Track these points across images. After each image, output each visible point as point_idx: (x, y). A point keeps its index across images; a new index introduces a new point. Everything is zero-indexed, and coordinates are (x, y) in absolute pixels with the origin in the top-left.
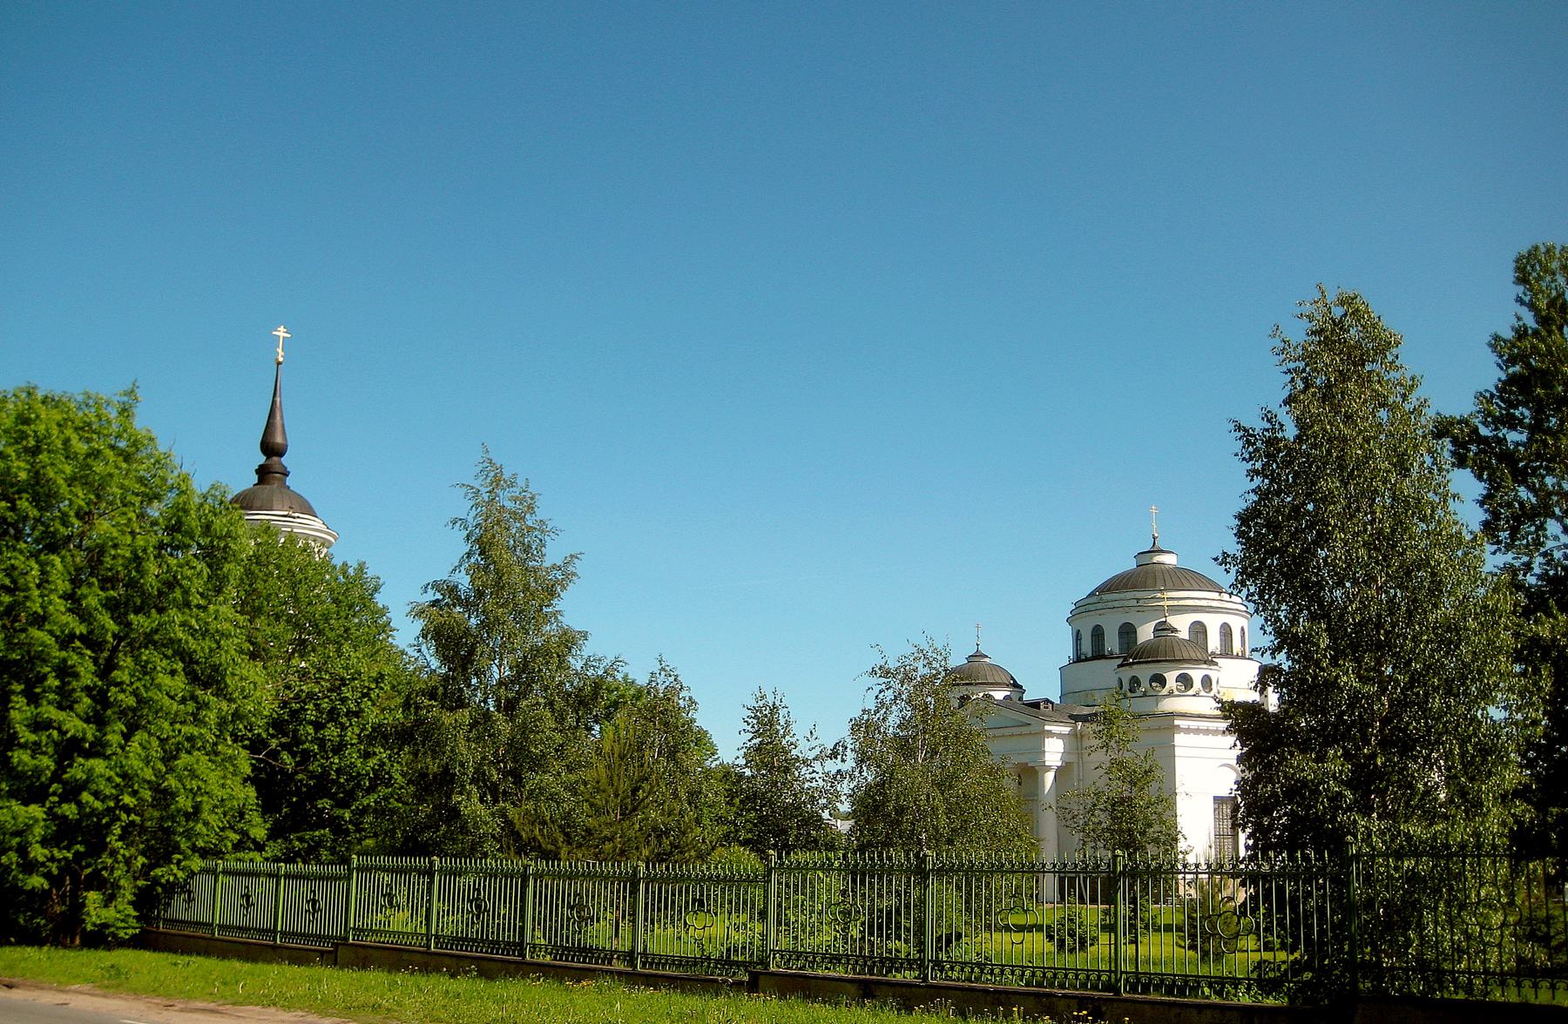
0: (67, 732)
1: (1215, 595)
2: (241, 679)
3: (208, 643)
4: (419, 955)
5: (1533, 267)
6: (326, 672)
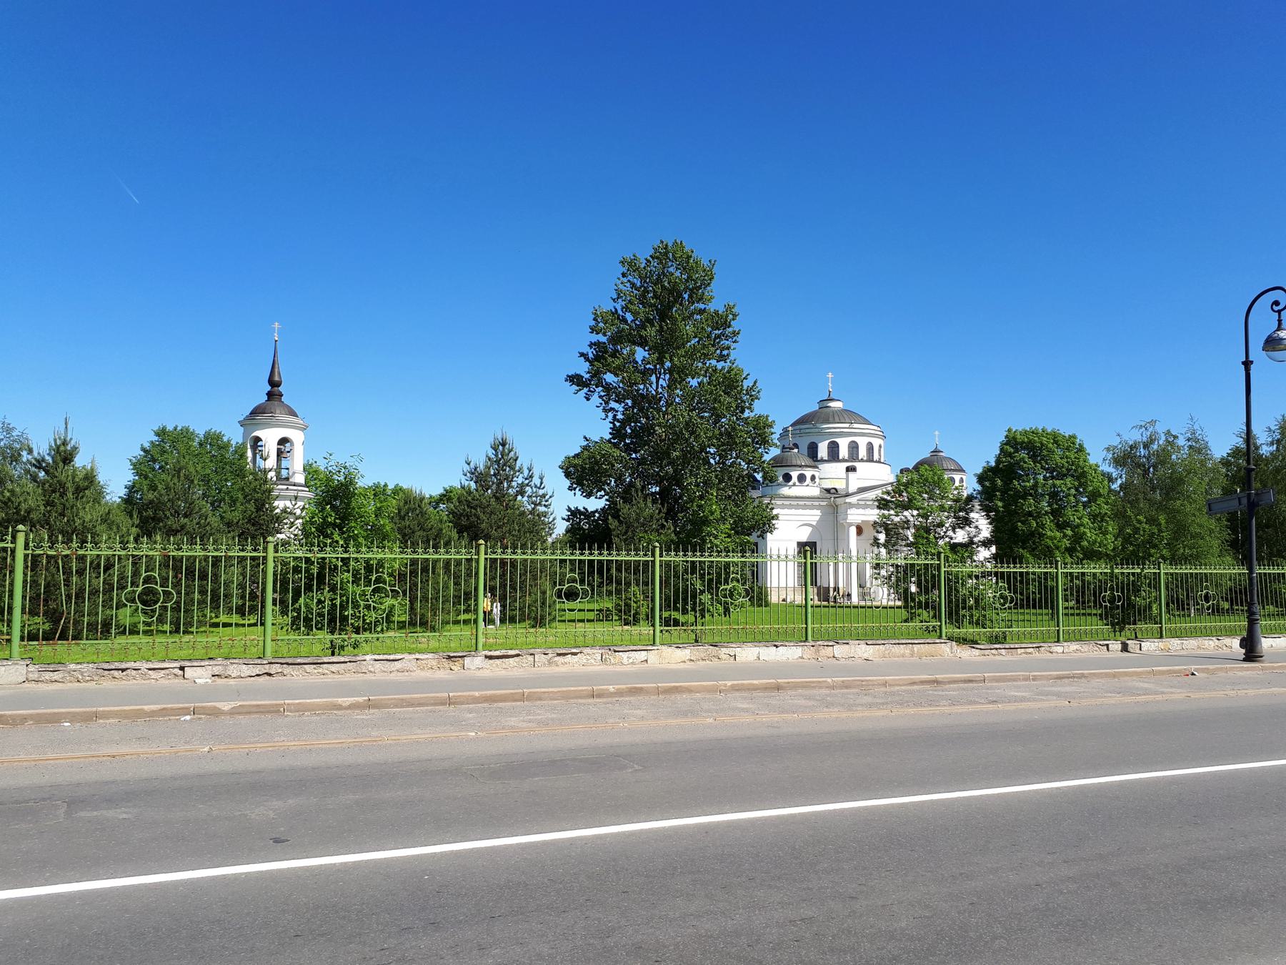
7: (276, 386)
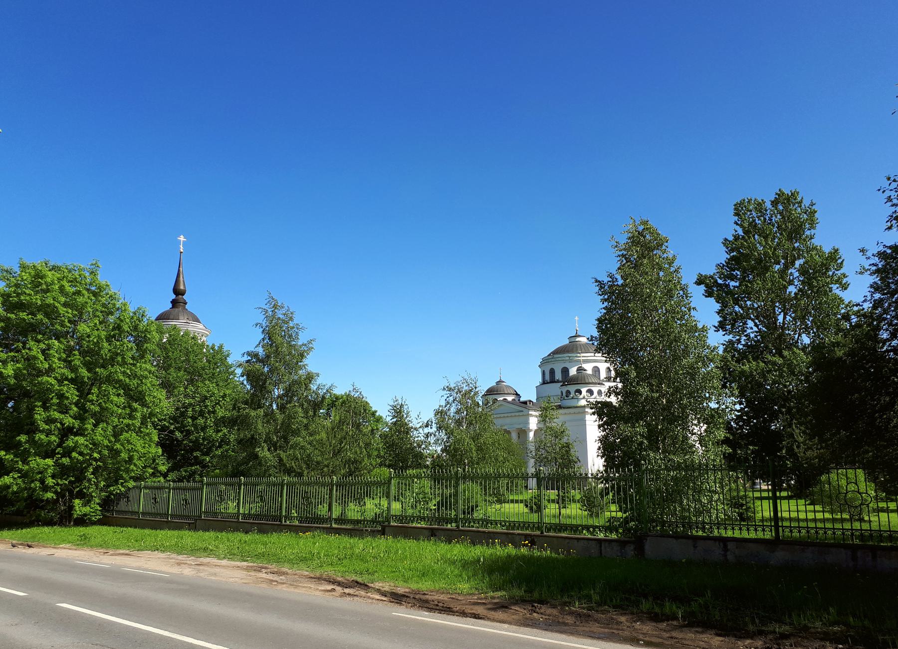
0: (65, 424)
3: (135, 382)
5: (742, 208)
6: (198, 393)
7: (181, 295)
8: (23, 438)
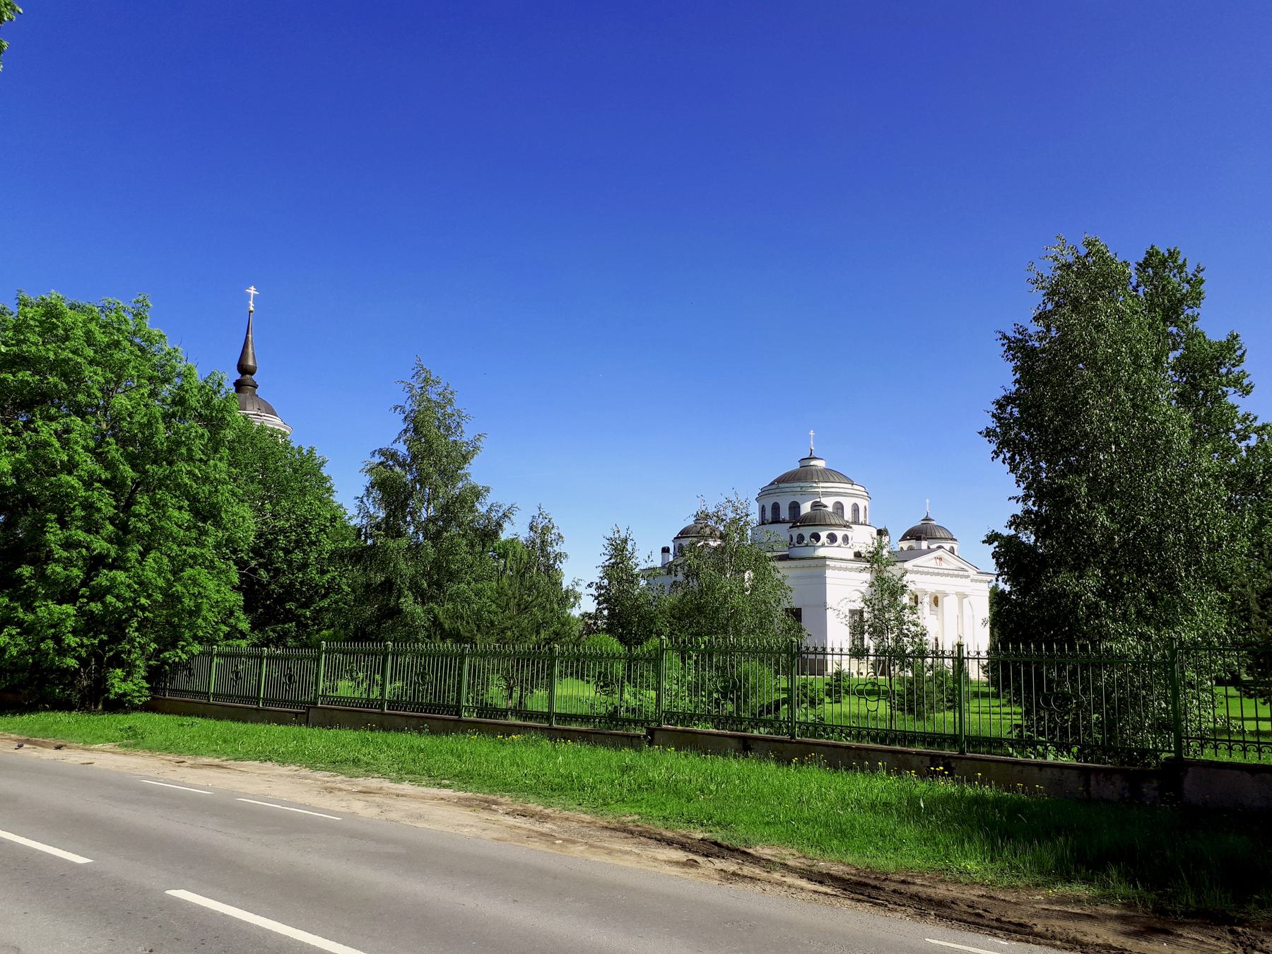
1: (850, 486)
2: (233, 515)
3: (206, 488)
4: (375, 715)
8: (26, 571)
